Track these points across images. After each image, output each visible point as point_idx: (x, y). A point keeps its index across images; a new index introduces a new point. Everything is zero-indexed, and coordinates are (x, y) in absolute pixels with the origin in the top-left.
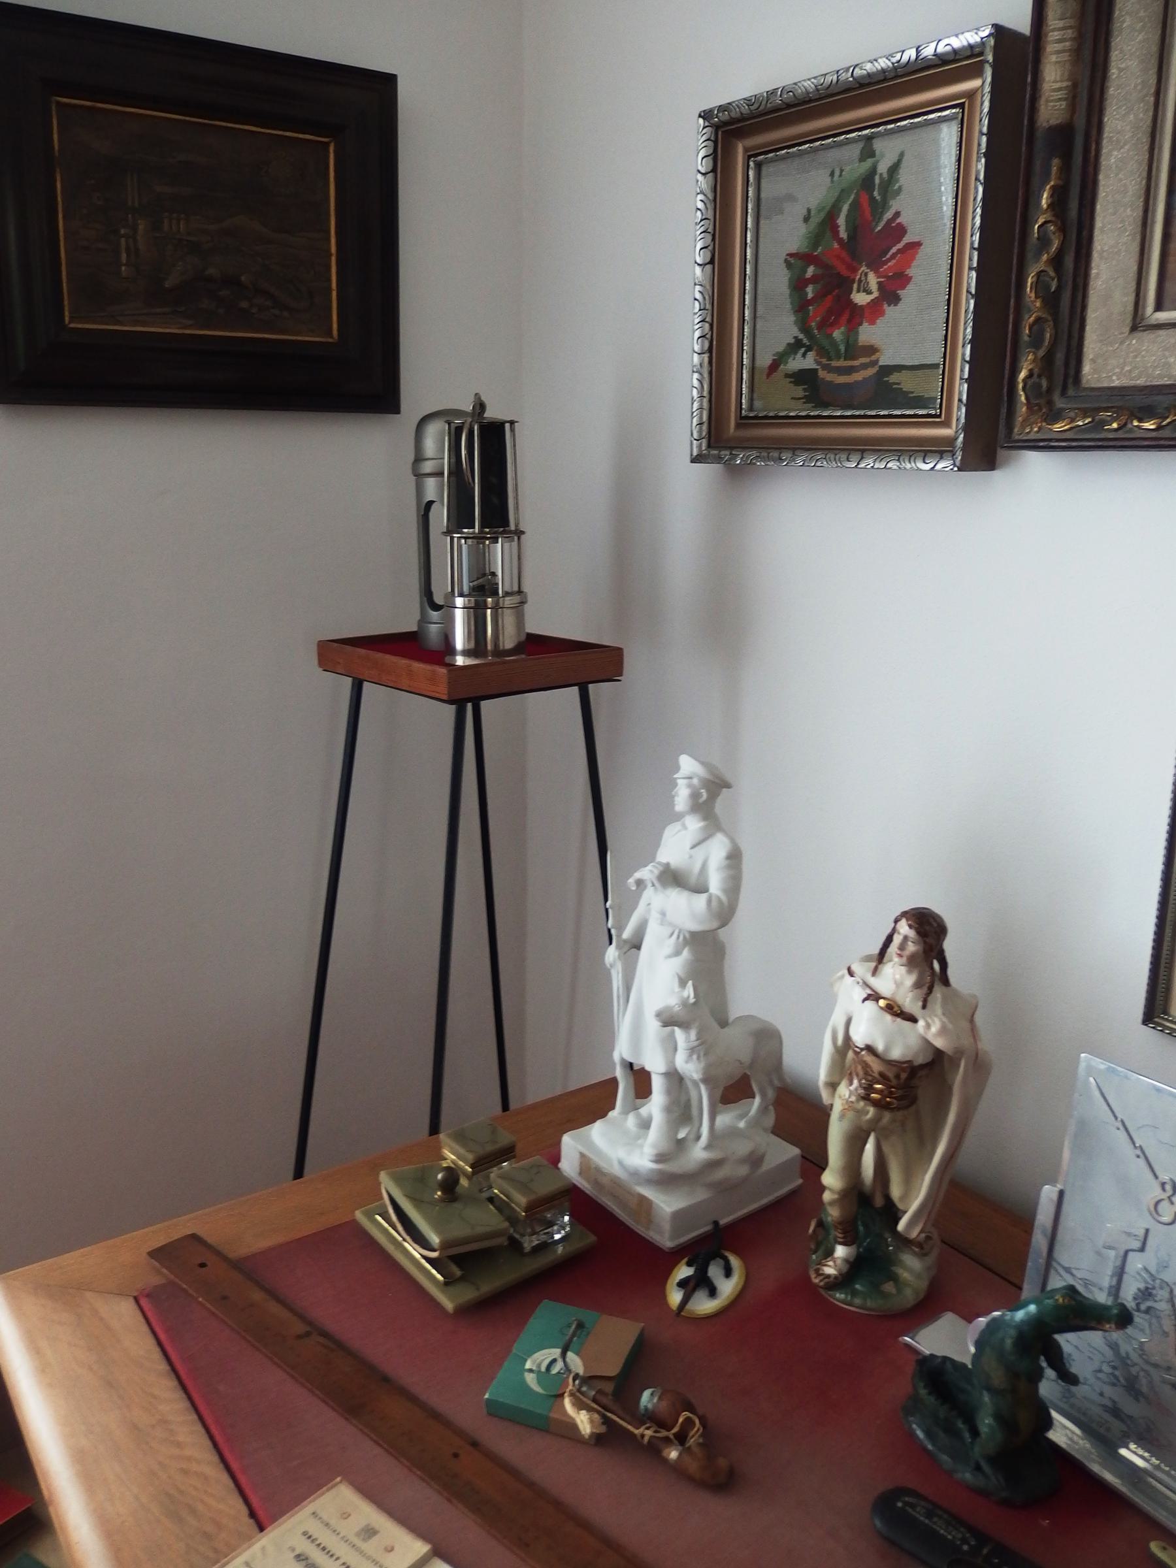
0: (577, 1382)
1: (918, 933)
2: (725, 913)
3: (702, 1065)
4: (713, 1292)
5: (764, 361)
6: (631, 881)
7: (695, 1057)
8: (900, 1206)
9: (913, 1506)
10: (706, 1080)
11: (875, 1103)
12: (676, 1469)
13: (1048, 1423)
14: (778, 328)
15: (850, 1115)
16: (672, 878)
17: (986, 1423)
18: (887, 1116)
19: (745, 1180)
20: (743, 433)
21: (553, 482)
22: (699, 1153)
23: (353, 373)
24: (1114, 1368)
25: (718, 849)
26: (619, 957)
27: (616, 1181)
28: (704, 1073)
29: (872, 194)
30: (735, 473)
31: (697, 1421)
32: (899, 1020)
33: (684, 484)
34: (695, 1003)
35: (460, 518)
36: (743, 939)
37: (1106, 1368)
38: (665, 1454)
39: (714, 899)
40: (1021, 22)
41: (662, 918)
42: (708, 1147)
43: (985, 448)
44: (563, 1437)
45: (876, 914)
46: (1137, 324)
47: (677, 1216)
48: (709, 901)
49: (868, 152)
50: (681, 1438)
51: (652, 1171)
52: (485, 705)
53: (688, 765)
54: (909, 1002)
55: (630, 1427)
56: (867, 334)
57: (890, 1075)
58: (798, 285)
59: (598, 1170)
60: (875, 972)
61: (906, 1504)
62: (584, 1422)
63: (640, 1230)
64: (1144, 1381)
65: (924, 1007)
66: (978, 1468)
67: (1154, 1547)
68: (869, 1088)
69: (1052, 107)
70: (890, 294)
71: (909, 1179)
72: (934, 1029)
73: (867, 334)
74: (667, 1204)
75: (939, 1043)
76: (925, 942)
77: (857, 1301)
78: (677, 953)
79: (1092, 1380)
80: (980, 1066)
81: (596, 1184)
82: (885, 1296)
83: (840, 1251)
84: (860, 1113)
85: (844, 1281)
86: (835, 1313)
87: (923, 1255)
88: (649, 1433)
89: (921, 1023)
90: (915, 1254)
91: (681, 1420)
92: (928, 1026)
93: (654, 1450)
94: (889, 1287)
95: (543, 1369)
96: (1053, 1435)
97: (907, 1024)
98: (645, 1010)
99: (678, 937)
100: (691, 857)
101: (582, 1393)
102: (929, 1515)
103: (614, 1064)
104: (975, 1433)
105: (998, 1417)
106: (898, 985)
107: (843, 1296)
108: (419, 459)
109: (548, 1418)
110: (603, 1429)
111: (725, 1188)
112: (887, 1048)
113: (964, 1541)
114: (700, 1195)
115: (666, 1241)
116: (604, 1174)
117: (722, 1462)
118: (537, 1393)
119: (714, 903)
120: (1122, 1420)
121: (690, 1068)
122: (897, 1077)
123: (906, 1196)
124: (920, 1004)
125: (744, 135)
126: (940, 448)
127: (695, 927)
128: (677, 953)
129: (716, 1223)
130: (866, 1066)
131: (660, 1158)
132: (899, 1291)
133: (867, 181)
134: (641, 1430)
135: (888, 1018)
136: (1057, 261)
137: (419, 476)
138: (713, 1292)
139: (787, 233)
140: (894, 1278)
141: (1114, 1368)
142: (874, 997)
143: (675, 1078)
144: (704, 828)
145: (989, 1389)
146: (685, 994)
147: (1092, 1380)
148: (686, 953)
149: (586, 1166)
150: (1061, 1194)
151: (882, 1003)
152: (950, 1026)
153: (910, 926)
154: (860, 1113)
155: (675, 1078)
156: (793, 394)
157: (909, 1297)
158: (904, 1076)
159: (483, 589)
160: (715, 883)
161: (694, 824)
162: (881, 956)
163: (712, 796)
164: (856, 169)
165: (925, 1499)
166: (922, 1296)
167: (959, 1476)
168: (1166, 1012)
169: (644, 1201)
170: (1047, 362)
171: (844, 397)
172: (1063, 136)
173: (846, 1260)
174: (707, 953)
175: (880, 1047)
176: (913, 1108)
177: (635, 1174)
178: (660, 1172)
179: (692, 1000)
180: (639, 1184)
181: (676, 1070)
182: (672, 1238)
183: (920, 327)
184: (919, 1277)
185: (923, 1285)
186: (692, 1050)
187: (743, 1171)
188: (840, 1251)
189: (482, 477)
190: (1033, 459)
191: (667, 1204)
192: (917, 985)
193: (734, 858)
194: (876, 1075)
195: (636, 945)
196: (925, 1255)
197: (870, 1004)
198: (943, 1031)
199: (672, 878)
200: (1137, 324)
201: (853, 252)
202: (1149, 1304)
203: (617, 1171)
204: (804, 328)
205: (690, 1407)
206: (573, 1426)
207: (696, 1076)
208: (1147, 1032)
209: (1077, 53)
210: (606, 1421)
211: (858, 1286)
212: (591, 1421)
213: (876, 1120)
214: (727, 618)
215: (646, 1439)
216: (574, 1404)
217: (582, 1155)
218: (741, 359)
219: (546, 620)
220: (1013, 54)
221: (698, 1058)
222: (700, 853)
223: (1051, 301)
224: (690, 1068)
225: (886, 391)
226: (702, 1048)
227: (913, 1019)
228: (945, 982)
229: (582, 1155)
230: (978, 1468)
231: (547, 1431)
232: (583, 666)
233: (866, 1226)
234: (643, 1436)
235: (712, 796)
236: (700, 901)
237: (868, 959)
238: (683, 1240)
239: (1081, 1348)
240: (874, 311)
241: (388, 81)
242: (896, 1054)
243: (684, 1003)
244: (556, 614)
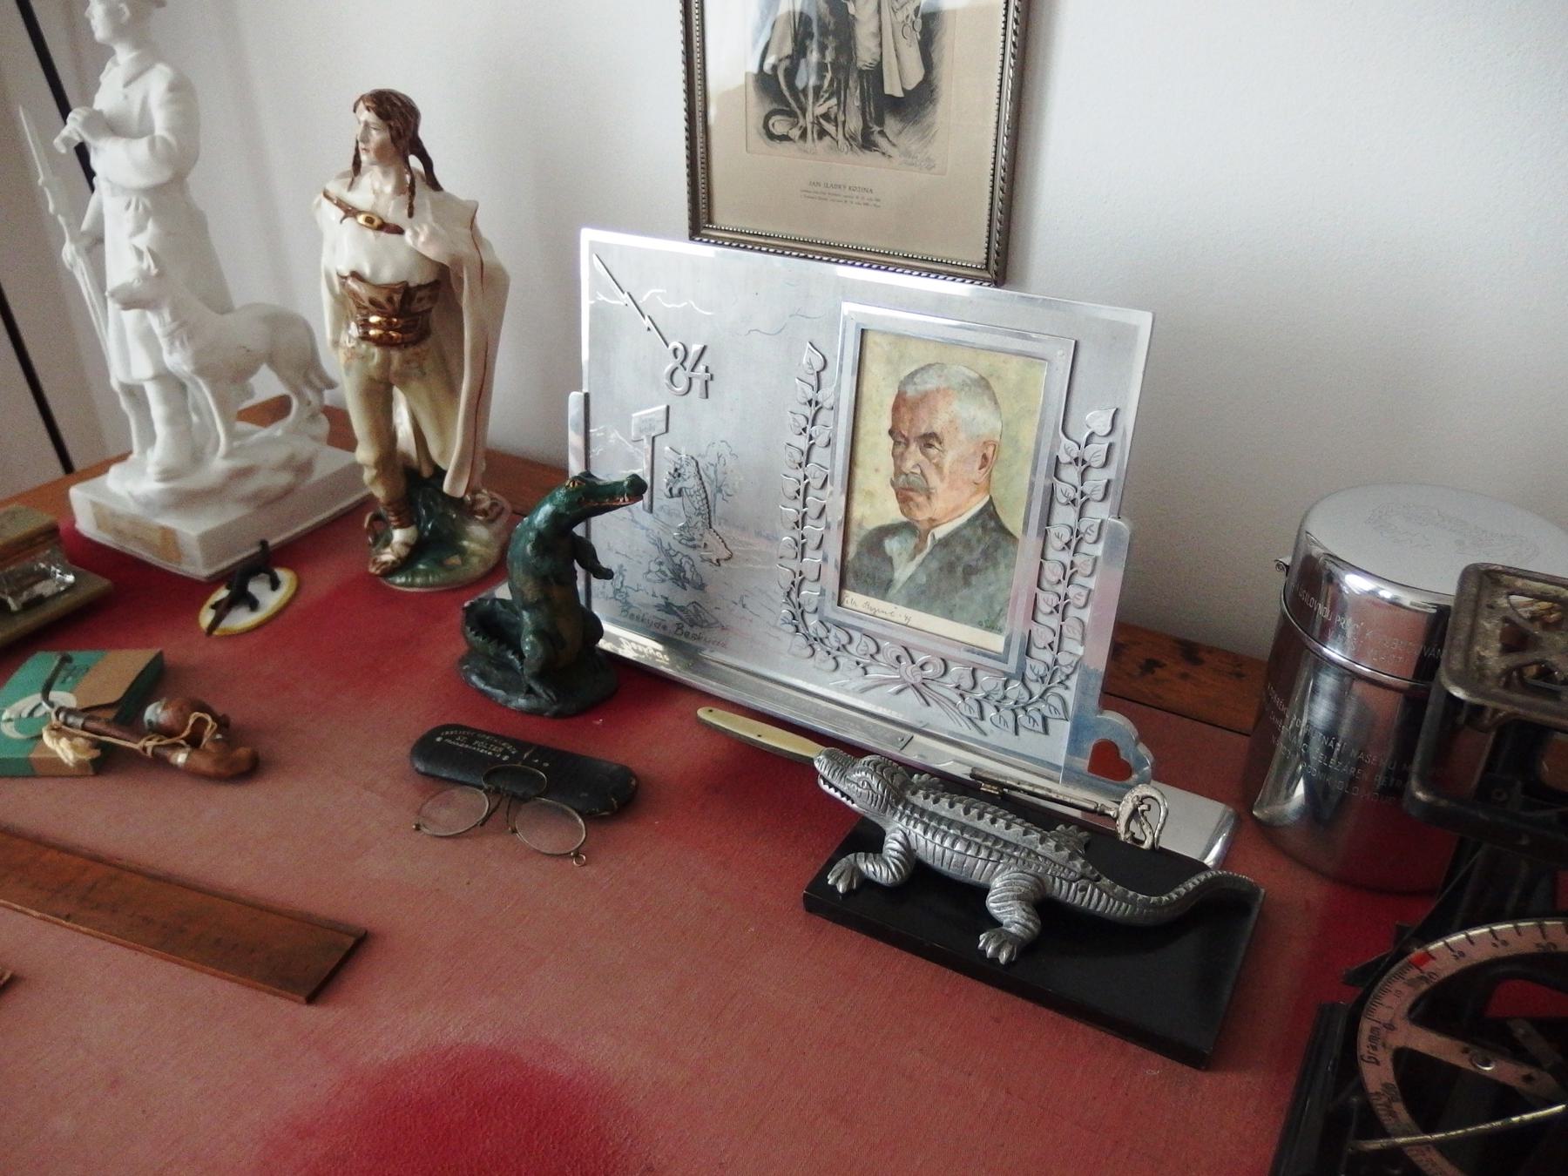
0: (61, 716)
1: (379, 115)
3: (190, 352)
4: (253, 605)
6: (57, 141)
7: (177, 343)
8: (443, 466)
9: (453, 738)
10: (201, 371)
11: (377, 341)
12: (189, 772)
13: (599, 633)
15: (356, 363)
17: (528, 643)
18: (396, 356)
19: (288, 491)
22: (219, 464)
24: (661, 564)
25: (157, 82)
26: (77, 250)
27: (134, 521)
28: (196, 363)
31: (209, 718)
32: (383, 234)
34: (159, 275)
37: (654, 567)
38: (172, 760)
39: (159, 145)
42: (229, 455)
44: (54, 776)
45: (355, 124)
47: (206, 539)
48: (152, 144)
50: (194, 742)
51: (162, 492)
54: (392, 211)
55: (129, 744)
57: (381, 299)
59: (113, 514)
60: (351, 186)
61: (445, 737)
62: (64, 750)
63: (171, 567)
64: (687, 567)
65: (411, 215)
66: (530, 691)
67: (702, 713)
68: (365, 325)
71: (443, 430)
72: (422, 238)
74: (190, 528)
75: (431, 252)
76: (391, 128)
77: (418, 580)
78: (140, 228)
79: (644, 584)
80: (492, 281)
81: (118, 532)
82: (451, 569)
83: (398, 535)
84: (365, 358)
85: (404, 565)
86: (396, 598)
87: (489, 522)
88: (150, 744)
89: (408, 233)
90: (481, 523)
91: (191, 722)
92: (416, 234)
93: (159, 762)
94: (455, 560)
95: (25, 715)
96: (603, 644)
97: (394, 237)
99: (137, 208)
100: (126, 97)
101: (70, 726)
102: (470, 742)
103: (114, 394)
104: (521, 657)
105: (539, 633)
106: (377, 194)
107: (403, 580)
109: (28, 760)
110: (96, 753)
111: (267, 501)
112: (375, 271)
113: (505, 752)
114: (232, 513)
115: (197, 567)
116: (120, 517)
117: (243, 752)
118: (18, 741)
119: (159, 145)
120: (675, 613)
121: (177, 361)
122: (390, 300)
123: (444, 453)
124: (406, 212)
127: (142, 181)
128: (140, 228)
129: (264, 543)
130: (354, 295)
131: (167, 475)
132: (464, 562)
134: (142, 743)
135: (370, 234)
138: (253, 605)
140: (462, 552)
141: (661, 564)
142: (350, 212)
143: (164, 377)
144: (138, 59)
145: (525, 608)
146: (145, 266)
147: (644, 584)
148: (150, 225)
149: (103, 517)
150: (587, 396)
151: (361, 219)
152: (442, 232)
153: (368, 109)
154: (365, 358)
155: (164, 377)
157: (476, 566)
158: (397, 298)
160: (160, 122)
161: (124, 55)
162: (357, 164)
165: (466, 728)
166: (491, 564)
167: (513, 705)
168: (710, 221)
169: (168, 534)
173: (405, 544)
174: (169, 198)
175: (366, 270)
176: (430, 341)
177: (147, 503)
178: (172, 492)
179: (154, 271)
180: (157, 516)
181: (166, 369)
182: (208, 564)
184: (487, 545)
185: (493, 552)
186: (171, 336)
187: (284, 479)
188: (398, 535)
191: (190, 528)
192: (399, 189)
193: (180, 89)
194: (367, 304)
196: (492, 521)
197: (348, 221)
198: (433, 236)
202: (679, 485)
203: (134, 509)
205: (204, 708)
206: (57, 762)
207: (382, 500)
208: (704, 252)
210: (98, 745)
211: (421, 567)
212: (74, 748)
213: (386, 363)
215: (149, 751)
216: (53, 737)
217: (94, 504)
221: (182, 343)
222: (136, 93)
224: (177, 361)
226: (184, 329)
227: (399, 231)
228: (434, 185)
229: (94, 504)
230: (530, 691)
231: (35, 776)
233: (428, 508)
234: (145, 749)
236: (141, 147)
237: (344, 175)
238: (225, 564)
239: (609, 533)
242: (387, 275)
243: (145, 276)
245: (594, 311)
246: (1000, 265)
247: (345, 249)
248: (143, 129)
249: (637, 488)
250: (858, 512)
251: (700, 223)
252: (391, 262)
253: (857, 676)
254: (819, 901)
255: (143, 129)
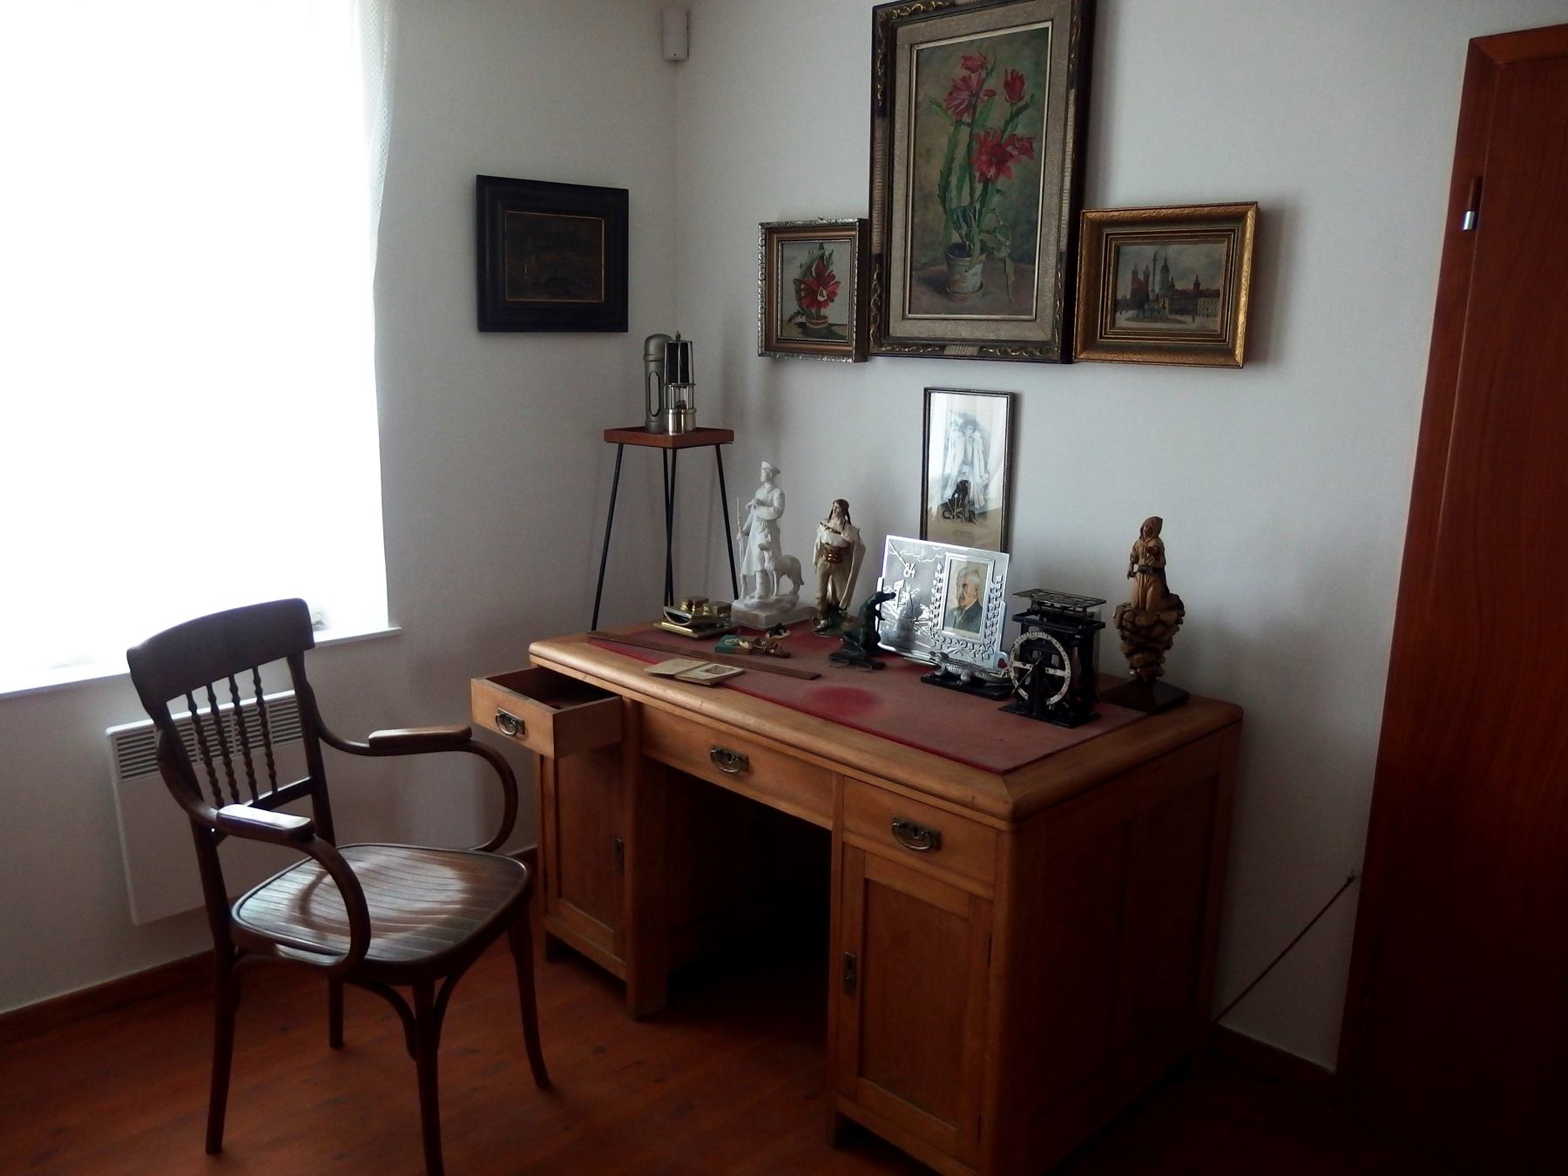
2: (780, 513)
5: (786, 317)
14: (792, 306)
16: (761, 503)
20: (776, 346)
21: (703, 363)
22: (773, 597)
23: (605, 313)
25: (776, 494)
27: (745, 613)
29: (823, 262)
30: (775, 361)
33: (754, 364)
35: (672, 379)
36: (783, 524)
40: (866, 216)
41: (757, 517)
43: (863, 355)
45: (830, 505)
46: (904, 318)
49: (821, 247)
52: (260, 668)
53: (765, 465)
54: (839, 528)
56: (823, 312)
58: (798, 291)
69: (876, 249)
70: (831, 298)
73: (823, 312)
80: (862, 549)
98: (753, 558)
108: (647, 354)
111: (784, 611)
125: (776, 235)
126: (846, 355)
133: (822, 257)
136: (880, 296)
137: (647, 362)
139: (793, 272)
155: (764, 572)
156: (796, 332)
159: (680, 406)
160: (776, 503)
161: (767, 486)
163: (774, 475)
164: (817, 253)
170: (879, 328)
171: (817, 334)
172: (880, 257)
174: (772, 526)
183: (840, 311)
189: (675, 360)
190: (879, 358)
191: (763, 614)
193: (782, 496)
195: (747, 534)
199: (761, 503)
200: (904, 318)
201: (816, 283)
204: (800, 305)
209: (882, 232)
214: (774, 418)
218: (777, 316)
219: (702, 421)
220: (864, 226)
223: (879, 309)
225: (830, 333)
226: (775, 557)
232: (718, 438)
235: (774, 475)
240: (825, 304)
241: (623, 194)
244: (705, 419)
245: (890, 556)
246: (1006, 547)
247: (824, 536)
248: (771, 505)
249: (893, 595)
250: (509, 991)
251: (924, 535)
252: (836, 541)
253: (938, 639)
254: (923, 680)
255: (771, 505)
